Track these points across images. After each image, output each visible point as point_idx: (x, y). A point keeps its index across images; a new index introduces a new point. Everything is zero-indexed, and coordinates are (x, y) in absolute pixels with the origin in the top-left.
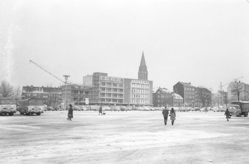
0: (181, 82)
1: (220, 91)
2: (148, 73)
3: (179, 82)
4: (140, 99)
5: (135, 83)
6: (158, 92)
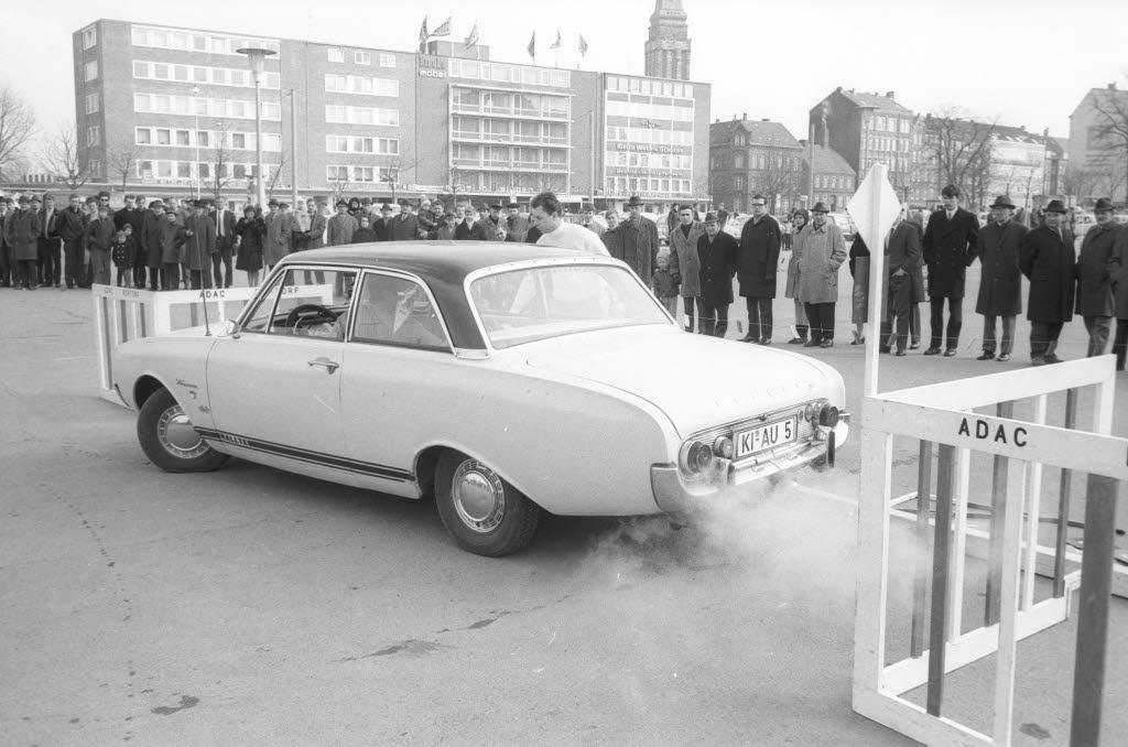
0: (846, 88)
3: (839, 89)
4: (668, 176)
6: (737, 140)
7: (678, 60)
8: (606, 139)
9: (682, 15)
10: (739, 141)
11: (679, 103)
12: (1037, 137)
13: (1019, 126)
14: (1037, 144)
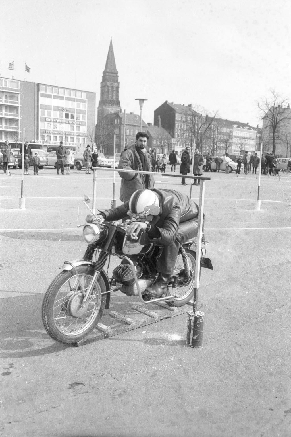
0: (170, 102)
1: (9, 365)
2: (120, 86)
3: (166, 102)
4: (74, 135)
5: (51, 95)
6: (116, 121)
7: (114, 91)
8: (40, 116)
9: (116, 72)
10: (117, 121)
11: (79, 101)
12: (254, 128)
13: (246, 123)
14: (253, 130)
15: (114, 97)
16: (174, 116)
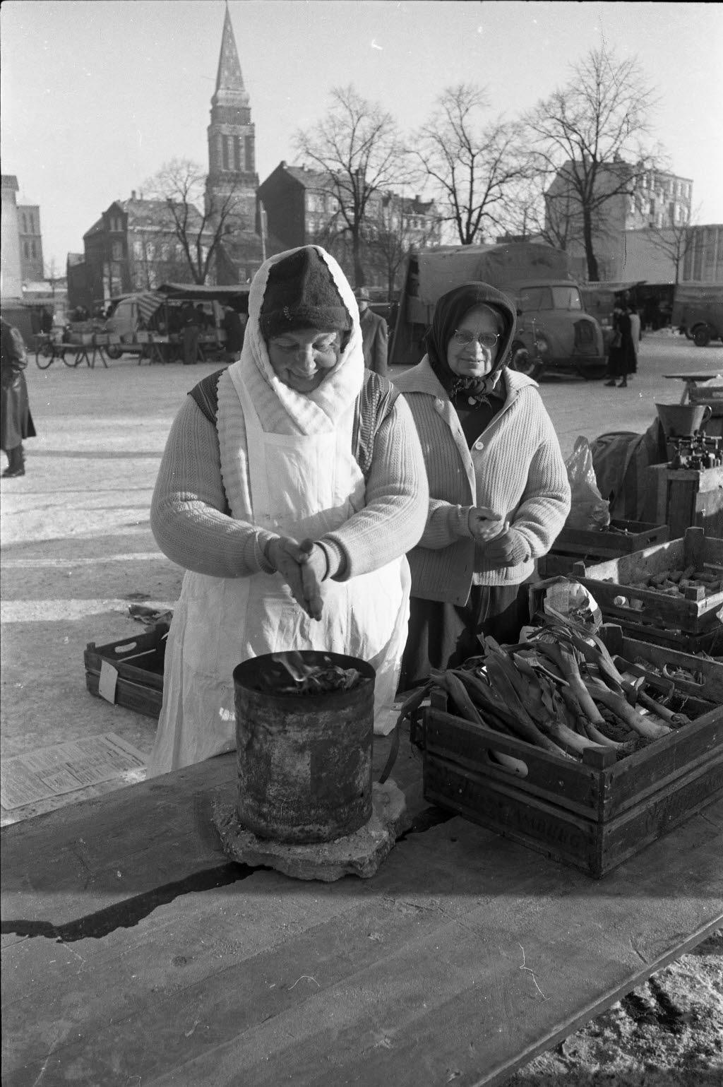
2: (257, 134)
3: (282, 163)
15: (243, 164)
16: (302, 204)
